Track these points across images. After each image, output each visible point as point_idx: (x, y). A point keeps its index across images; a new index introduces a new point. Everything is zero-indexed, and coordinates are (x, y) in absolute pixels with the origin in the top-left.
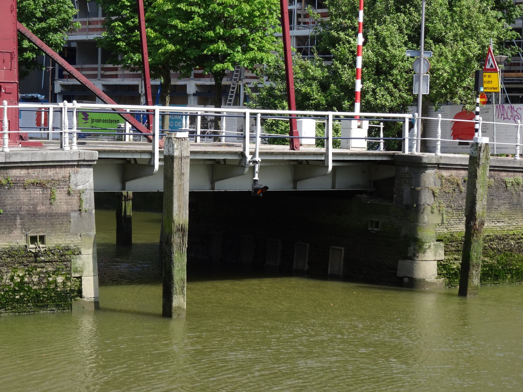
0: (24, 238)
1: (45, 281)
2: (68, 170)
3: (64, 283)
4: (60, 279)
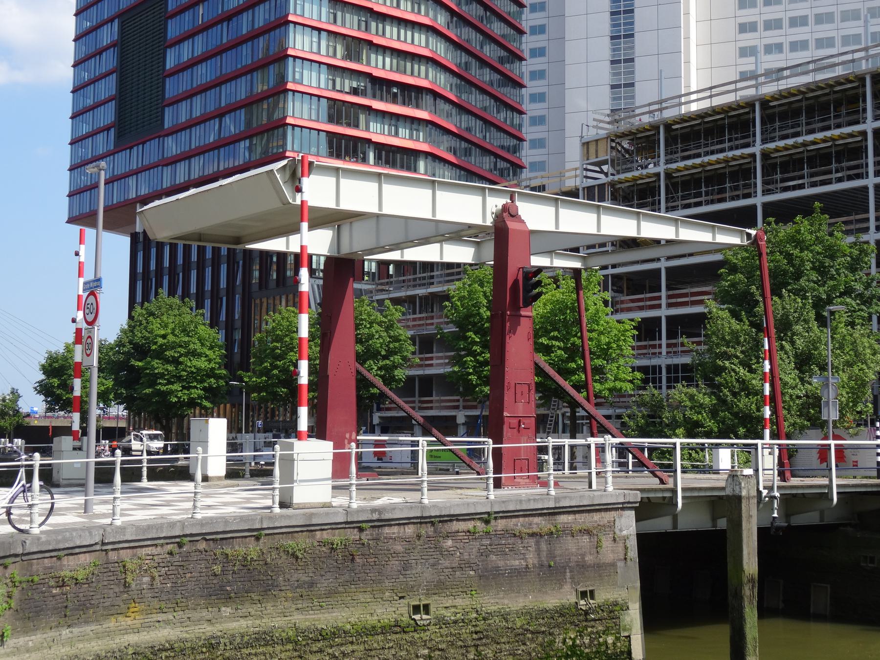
0: (574, 593)
1: (596, 643)
2: (613, 514)
3: (614, 643)
4: (610, 640)
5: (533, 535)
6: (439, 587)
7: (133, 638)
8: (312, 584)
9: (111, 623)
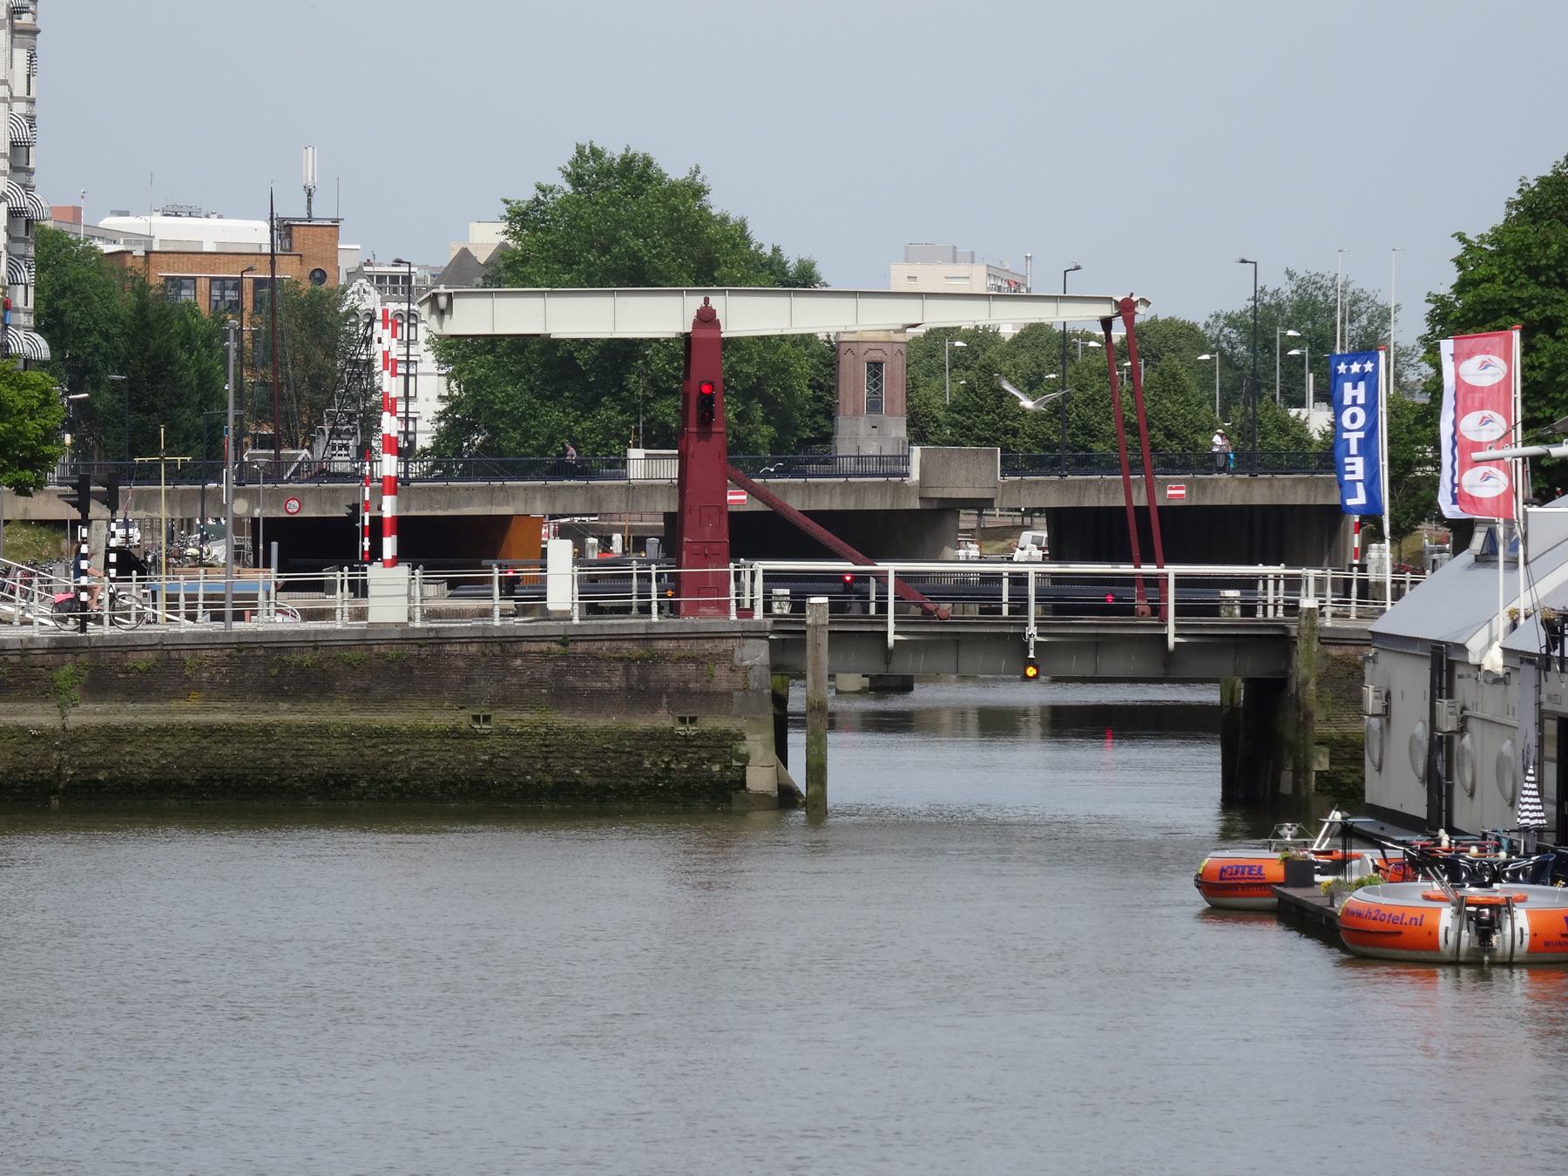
5: (621, 659)
6: (505, 702)
7: (193, 718)
8: (367, 690)
9: (174, 704)
